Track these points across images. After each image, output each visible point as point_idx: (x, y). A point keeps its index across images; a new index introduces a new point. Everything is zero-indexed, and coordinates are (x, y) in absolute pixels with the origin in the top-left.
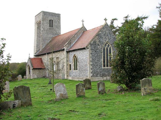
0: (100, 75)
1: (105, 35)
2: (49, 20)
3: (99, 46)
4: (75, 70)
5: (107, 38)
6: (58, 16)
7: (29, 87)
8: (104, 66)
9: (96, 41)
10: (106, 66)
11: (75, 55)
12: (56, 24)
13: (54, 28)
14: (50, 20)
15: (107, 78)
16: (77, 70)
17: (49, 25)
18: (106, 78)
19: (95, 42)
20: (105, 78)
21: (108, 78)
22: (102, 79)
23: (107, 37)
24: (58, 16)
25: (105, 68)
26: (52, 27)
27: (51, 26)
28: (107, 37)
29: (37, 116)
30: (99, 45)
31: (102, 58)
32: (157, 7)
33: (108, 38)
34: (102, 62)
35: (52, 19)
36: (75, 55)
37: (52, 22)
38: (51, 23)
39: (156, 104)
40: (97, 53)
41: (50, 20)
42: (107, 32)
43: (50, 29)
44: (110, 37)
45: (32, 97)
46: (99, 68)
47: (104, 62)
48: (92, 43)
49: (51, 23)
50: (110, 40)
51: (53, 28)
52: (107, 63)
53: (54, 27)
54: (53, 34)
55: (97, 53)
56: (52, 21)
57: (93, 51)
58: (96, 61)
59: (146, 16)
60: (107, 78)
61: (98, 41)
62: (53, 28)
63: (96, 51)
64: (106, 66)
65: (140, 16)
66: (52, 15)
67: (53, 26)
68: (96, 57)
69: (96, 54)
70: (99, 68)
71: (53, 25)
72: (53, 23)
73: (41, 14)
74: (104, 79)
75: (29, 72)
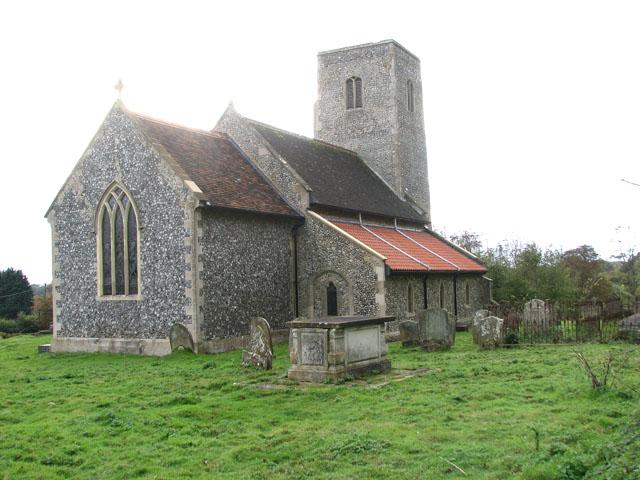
0: (89, 329)
1: (107, 155)
2: (343, 81)
3: (84, 211)
4: (120, 291)
5: (119, 169)
6: (329, 59)
7: (51, 333)
8: (107, 291)
9: (74, 192)
10: (114, 290)
15: (113, 342)
16: (133, 290)
17: (344, 104)
18: (108, 345)
19: (71, 195)
20: (105, 344)
21: (118, 345)
22: (93, 344)
23: (117, 164)
24: (329, 59)
25: (110, 298)
26: (359, 105)
27: (352, 102)
28: (117, 164)
30: (83, 205)
31: (95, 255)
33: (122, 167)
34: (95, 274)
35: (357, 72)
40: (76, 241)
41: (349, 81)
42: (117, 141)
43: (349, 116)
44: (131, 157)
46: (86, 298)
47: (106, 273)
48: (60, 202)
50: (128, 172)
52: (119, 277)
55: (78, 238)
56: (358, 79)
57: (64, 234)
58: (74, 273)
60: (113, 342)
61: (82, 188)
63: (72, 233)
64: (114, 290)
66: (357, 57)
68: (72, 257)
69: (73, 245)
70: (86, 298)
71: (363, 96)
74: (101, 348)
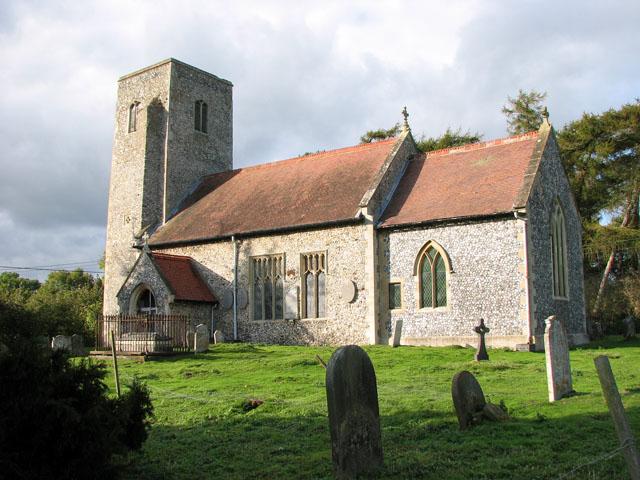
11: (433, 244)
12: (217, 121)
13: (211, 137)
14: (197, 103)
29: (206, 463)
32: (506, 111)
35: (205, 98)
36: (430, 242)
37: (205, 112)
38: (201, 113)
39: (407, 385)
41: (197, 103)
43: (196, 137)
45: (599, 395)
49: (201, 113)
51: (207, 137)
53: (211, 133)
54: (206, 161)
56: (205, 105)
59: (472, 135)
62: (207, 137)
65: (453, 132)
67: (209, 128)
71: (208, 124)
72: (208, 117)
73: (169, 66)
75: (309, 304)
